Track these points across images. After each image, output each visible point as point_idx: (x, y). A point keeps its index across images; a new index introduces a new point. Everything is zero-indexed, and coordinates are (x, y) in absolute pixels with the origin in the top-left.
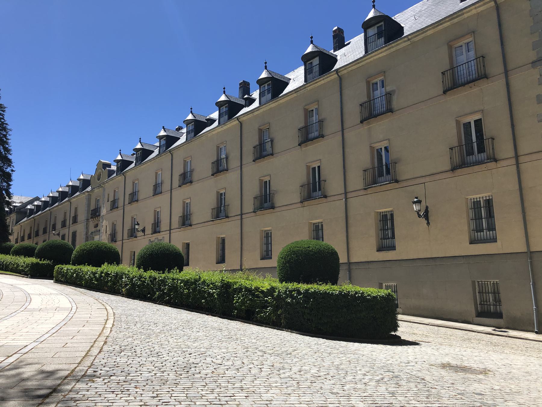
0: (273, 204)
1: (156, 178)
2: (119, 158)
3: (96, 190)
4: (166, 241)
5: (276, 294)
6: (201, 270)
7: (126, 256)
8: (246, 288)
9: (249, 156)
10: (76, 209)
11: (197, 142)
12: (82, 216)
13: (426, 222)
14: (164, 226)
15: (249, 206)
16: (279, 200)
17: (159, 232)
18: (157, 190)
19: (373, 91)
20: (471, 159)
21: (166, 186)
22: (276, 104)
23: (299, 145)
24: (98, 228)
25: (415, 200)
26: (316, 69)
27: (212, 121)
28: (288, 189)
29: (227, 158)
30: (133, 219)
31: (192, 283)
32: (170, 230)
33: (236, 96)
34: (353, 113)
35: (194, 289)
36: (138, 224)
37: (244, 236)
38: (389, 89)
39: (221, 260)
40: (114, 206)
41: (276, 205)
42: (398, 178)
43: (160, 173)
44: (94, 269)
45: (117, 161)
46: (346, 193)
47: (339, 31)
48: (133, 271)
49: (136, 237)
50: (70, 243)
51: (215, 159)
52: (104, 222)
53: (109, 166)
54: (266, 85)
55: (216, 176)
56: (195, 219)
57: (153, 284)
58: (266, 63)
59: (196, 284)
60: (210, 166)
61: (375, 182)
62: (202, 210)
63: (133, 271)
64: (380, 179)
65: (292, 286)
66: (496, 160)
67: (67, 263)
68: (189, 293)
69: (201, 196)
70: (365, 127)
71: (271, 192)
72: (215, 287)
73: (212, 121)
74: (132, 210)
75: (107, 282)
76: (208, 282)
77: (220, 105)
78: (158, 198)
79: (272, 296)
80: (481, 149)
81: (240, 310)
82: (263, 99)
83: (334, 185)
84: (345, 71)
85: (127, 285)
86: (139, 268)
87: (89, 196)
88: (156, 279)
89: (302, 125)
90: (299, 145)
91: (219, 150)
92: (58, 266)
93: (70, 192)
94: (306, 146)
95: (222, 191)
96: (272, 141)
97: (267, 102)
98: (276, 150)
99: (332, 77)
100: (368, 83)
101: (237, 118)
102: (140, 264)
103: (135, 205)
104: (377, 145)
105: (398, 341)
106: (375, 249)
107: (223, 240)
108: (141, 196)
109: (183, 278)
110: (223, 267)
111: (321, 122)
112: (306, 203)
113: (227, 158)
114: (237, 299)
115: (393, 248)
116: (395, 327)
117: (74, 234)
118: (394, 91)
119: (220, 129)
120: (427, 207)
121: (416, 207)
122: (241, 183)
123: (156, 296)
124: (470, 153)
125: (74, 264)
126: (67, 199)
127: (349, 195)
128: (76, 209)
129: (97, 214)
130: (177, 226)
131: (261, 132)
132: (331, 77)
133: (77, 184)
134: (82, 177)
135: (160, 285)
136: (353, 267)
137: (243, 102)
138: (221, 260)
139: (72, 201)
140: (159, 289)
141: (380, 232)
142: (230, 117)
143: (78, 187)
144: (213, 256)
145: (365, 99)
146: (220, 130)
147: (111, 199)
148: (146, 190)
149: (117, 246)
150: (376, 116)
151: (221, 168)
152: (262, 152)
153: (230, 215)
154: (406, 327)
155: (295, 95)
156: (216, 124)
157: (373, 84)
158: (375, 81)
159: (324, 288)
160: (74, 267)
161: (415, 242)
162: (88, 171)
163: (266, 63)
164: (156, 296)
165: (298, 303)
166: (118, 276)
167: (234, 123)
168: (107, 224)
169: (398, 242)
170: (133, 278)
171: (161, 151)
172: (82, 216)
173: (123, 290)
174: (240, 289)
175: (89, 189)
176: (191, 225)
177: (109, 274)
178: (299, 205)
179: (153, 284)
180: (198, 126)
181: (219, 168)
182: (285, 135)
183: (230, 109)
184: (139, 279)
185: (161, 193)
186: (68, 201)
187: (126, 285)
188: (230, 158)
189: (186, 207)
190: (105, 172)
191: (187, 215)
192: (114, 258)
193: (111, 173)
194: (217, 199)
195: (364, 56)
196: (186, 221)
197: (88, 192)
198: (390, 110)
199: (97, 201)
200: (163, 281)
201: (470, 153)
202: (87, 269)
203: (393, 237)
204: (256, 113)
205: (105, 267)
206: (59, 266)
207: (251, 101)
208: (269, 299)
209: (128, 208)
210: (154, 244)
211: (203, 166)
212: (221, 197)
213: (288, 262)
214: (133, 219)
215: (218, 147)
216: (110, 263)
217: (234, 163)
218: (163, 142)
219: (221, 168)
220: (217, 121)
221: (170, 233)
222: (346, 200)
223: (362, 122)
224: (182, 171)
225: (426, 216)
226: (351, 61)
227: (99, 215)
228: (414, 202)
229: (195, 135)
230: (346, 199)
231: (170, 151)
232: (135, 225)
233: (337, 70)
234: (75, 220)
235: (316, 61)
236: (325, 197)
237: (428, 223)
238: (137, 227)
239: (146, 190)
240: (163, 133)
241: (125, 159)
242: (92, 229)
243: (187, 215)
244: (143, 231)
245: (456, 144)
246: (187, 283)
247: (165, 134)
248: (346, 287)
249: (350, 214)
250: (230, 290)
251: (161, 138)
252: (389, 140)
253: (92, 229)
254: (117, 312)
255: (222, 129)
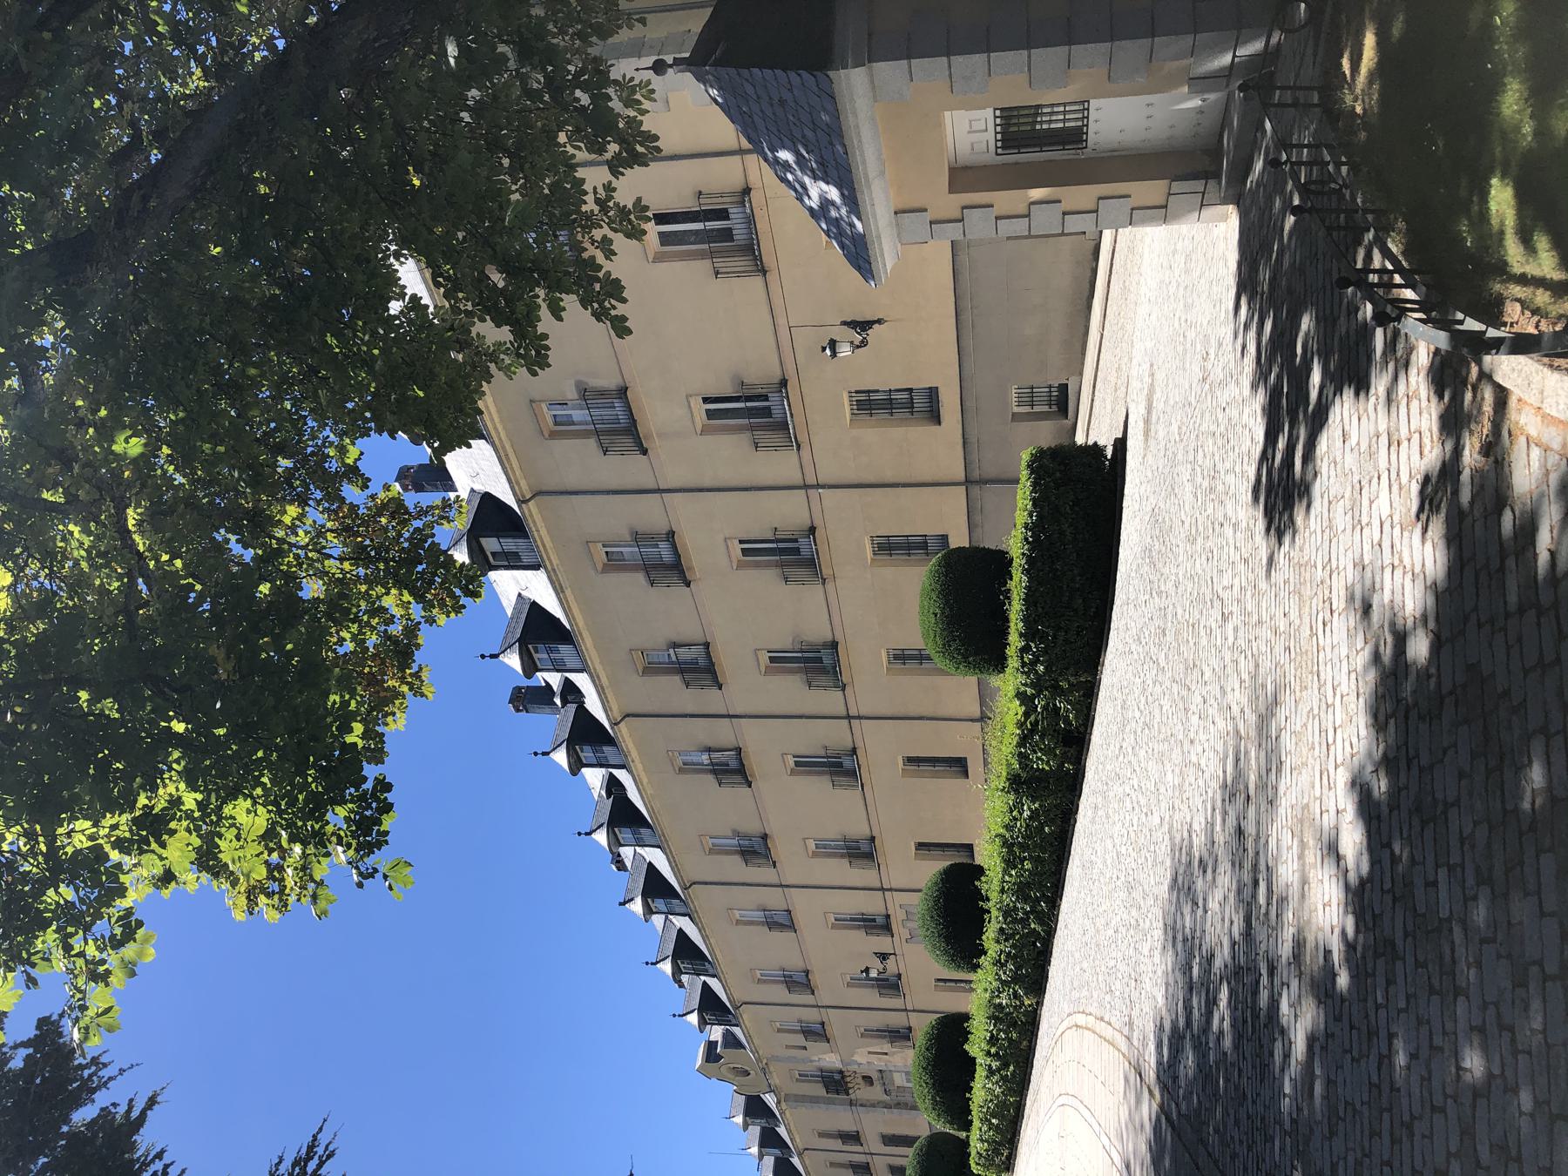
0: (825, 645)
1: (751, 923)
2: (693, 1018)
3: (775, 1080)
4: (915, 900)
5: (1029, 691)
6: (984, 818)
7: (951, 1003)
8: (1019, 745)
9: (710, 699)
10: (822, 1135)
11: (665, 823)
12: (843, 1119)
13: (876, 326)
14: (871, 904)
15: (830, 700)
16: (817, 631)
17: (888, 916)
18: (782, 922)
19: (573, 423)
20: (740, 233)
21: (774, 899)
22: (586, 634)
23: (688, 584)
24: (875, 1076)
25: (828, 352)
26: (510, 544)
27: (613, 786)
28: (797, 612)
29: (709, 750)
30: (854, 983)
31: (1011, 851)
32: (882, 889)
33: (559, 721)
34: (624, 468)
35: (1023, 847)
36: (867, 970)
37: (902, 712)
38: (571, 394)
39: (959, 766)
40: (817, 1033)
41: (830, 638)
42: (776, 380)
43: (737, 913)
44: (980, 1073)
45: (703, 1022)
46: (806, 487)
47: (406, 477)
48: (985, 978)
49: (899, 976)
50: (910, 1151)
51: (711, 777)
52: (857, 1058)
53: (711, 1046)
54: (536, 656)
55: (753, 775)
56: (859, 829)
57: (1013, 936)
58: (483, 656)
59: (1013, 845)
60: (727, 791)
61: (784, 426)
62: (833, 809)
63: (985, 978)
64: (776, 411)
65: (1011, 651)
66: (747, 191)
67: (965, 1144)
68: (1031, 858)
69: (800, 811)
70: (655, 445)
71: (798, 647)
72: (1018, 805)
73: (613, 786)
74: (830, 986)
75: (1010, 1040)
76: (1007, 820)
77: (576, 765)
78: (800, 918)
79: (1033, 697)
80: (723, 214)
81: (1065, 758)
82: (572, 662)
83: (787, 512)
84: (523, 483)
85: (1015, 993)
86: (978, 966)
87: (787, 1098)
88: (1001, 929)
89: (640, 577)
90: (688, 584)
91: (688, 768)
92: (973, 1165)
93: (777, 1151)
94: (691, 568)
95: (791, 761)
96: (675, 645)
97: (579, 653)
98: (699, 638)
99: (535, 511)
100: (553, 435)
101: (614, 724)
102: (1320, 203)
103: (816, 979)
104: (698, 420)
105: (1121, 445)
106: (935, 428)
107: (910, 760)
108: (794, 962)
109: (999, 870)
110: (975, 767)
111: (638, 538)
112: (826, 572)
113: (709, 750)
114: (1041, 763)
115: (933, 394)
116: (1096, 450)
117: (891, 1140)
118: (578, 384)
119: (638, 766)
120: (844, 323)
121: (845, 350)
122: (773, 718)
123: (1039, 929)
124: (727, 235)
125: (967, 1126)
126: (795, 1161)
127: (811, 480)
128: (822, 1135)
129: (837, 1077)
130: (875, 872)
131: (651, 669)
132: (534, 515)
133: (755, 1131)
134: (739, 1119)
135: (1015, 921)
136: (976, 475)
137: (572, 708)
138: (959, 766)
139: (801, 1147)
140: (1024, 922)
141: (896, 416)
142: (610, 741)
143: (763, 1130)
144: (950, 785)
145: (592, 443)
146: (640, 766)
147: (800, 1040)
148: (779, 951)
149: (922, 1026)
150: (633, 421)
151: (733, 764)
152: (700, 668)
153: (850, 745)
154: (1095, 430)
155: (568, 592)
156: (621, 775)
157: (556, 424)
158: (550, 421)
159: (1018, 583)
160: (976, 1123)
161: (919, 349)
162: (726, 1099)
163: (483, 656)
164: (1039, 929)
165: (1045, 652)
166: (998, 1015)
167: (624, 734)
168: (864, 1050)
169: (921, 382)
170: (999, 979)
171: (683, 910)
172: (843, 1119)
173: (1027, 1002)
174: (1022, 757)
175: (770, 1100)
176: (873, 839)
177: (992, 1036)
178: (830, 586)
179: (1013, 936)
180: (623, 816)
181: (732, 769)
182: (664, 615)
183: (588, 737)
184: (1002, 965)
185: (789, 911)
186: (800, 1155)
187: (1016, 995)
188: (711, 744)
189: (824, 849)
190: (729, 1055)
191: (848, 848)
192: (952, 1029)
193: (731, 1041)
194: (809, 773)
195: (493, 444)
196: (862, 851)
197: (779, 1102)
198: (623, 392)
199: (804, 1077)
200: (1007, 913)
201: (727, 235)
202: (981, 1091)
203: (910, 390)
204: (604, 681)
205: (976, 1048)
206: (972, 1162)
207: (570, 690)
208: (1040, 704)
209: (824, 997)
210: (922, 932)
211: (728, 809)
212: (805, 765)
213: (965, 657)
214: (854, 983)
215: (681, 771)
216: (965, 1035)
217: (723, 733)
218: (659, 904)
219: (733, 764)
220: (616, 772)
221: (890, 890)
222: (823, 487)
223: (645, 452)
224: (737, 859)
225: (863, 326)
226: (498, 469)
227: (841, 1072)
228: (834, 354)
229: (648, 826)
230: (818, 486)
231: (685, 888)
232: (868, 978)
233: (520, 502)
234: (853, 1138)
235: (490, 544)
236: (812, 530)
237: (879, 321)
238: (873, 974)
239: (779, 951)
240: (637, 906)
241: (695, 1003)
242: (876, 1093)
243: (848, 848)
244: (883, 957)
245: (707, 263)
246: (1009, 863)
247: (639, 900)
248: (1016, 546)
249: (853, 477)
250: (1024, 775)
251: (649, 911)
252: (688, 396)
253: (876, 1093)
254: (1067, 1009)
255: (637, 760)
